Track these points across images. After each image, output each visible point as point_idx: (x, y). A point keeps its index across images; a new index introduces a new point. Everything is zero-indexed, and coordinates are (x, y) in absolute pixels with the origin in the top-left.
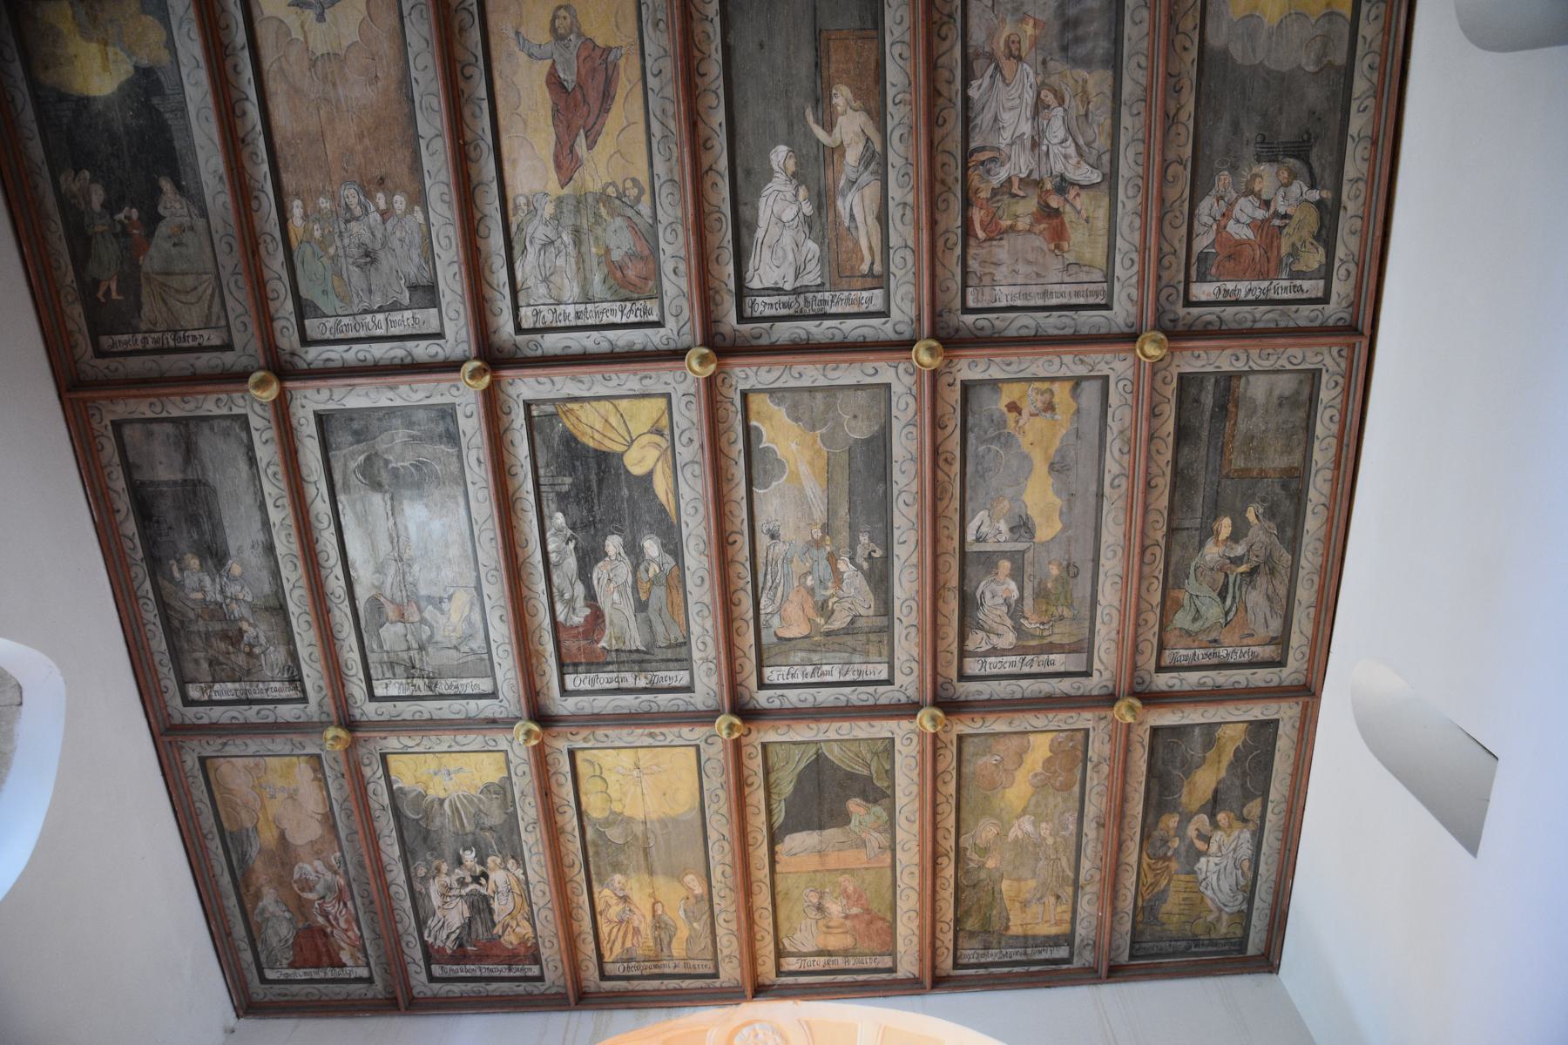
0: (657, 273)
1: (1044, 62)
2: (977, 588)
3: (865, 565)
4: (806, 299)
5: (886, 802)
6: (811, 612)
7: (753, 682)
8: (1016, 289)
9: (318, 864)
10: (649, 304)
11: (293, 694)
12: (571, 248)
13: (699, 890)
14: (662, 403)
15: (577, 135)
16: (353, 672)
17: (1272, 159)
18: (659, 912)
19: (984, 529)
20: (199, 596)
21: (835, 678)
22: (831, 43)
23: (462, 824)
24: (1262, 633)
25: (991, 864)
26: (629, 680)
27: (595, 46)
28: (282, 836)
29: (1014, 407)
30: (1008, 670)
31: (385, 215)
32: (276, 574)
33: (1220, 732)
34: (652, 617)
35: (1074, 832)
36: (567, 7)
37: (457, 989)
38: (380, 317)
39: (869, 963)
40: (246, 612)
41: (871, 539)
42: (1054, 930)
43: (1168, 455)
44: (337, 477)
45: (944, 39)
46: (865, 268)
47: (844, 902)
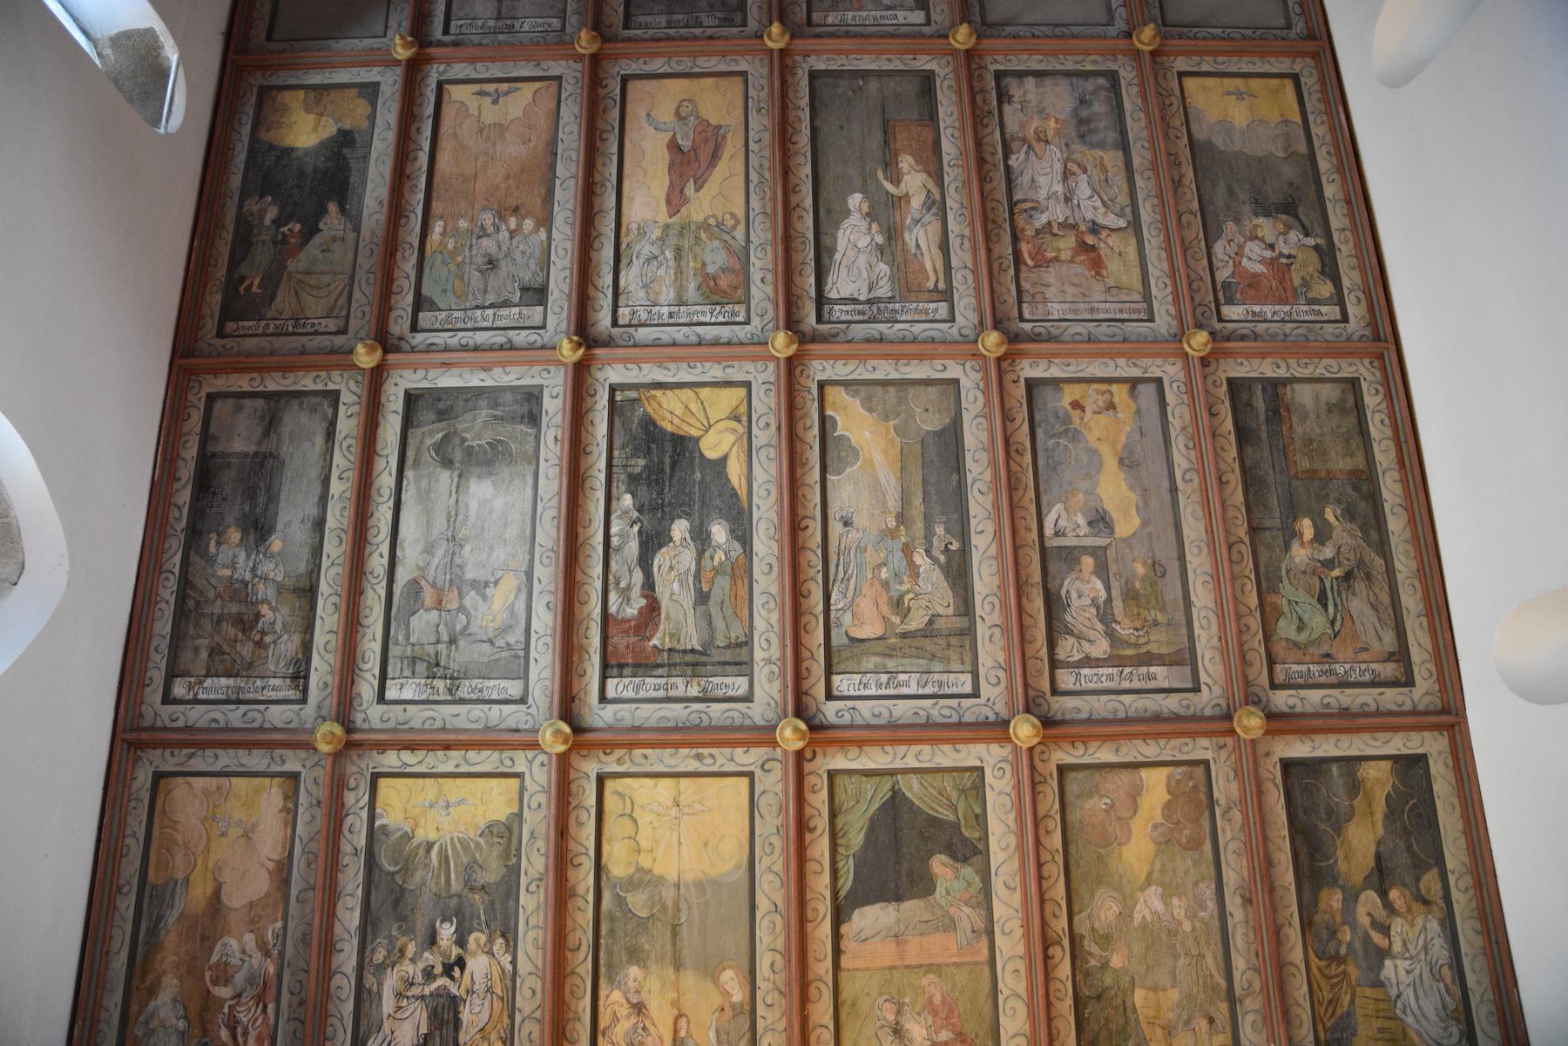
2: (1061, 586)
3: (942, 558)
4: (878, 308)
6: (886, 609)
10: (737, 308)
12: (671, 263)
13: (738, 995)
14: (742, 392)
18: (683, 1033)
19: (1062, 523)
21: (912, 690)
24: (1376, 646)
25: (1116, 961)
27: (709, 124)
29: (1076, 405)
32: (317, 551)
35: (1216, 913)
36: (689, 101)
38: (490, 312)
40: (271, 593)
41: (947, 531)
46: (931, 285)
47: (930, 1019)
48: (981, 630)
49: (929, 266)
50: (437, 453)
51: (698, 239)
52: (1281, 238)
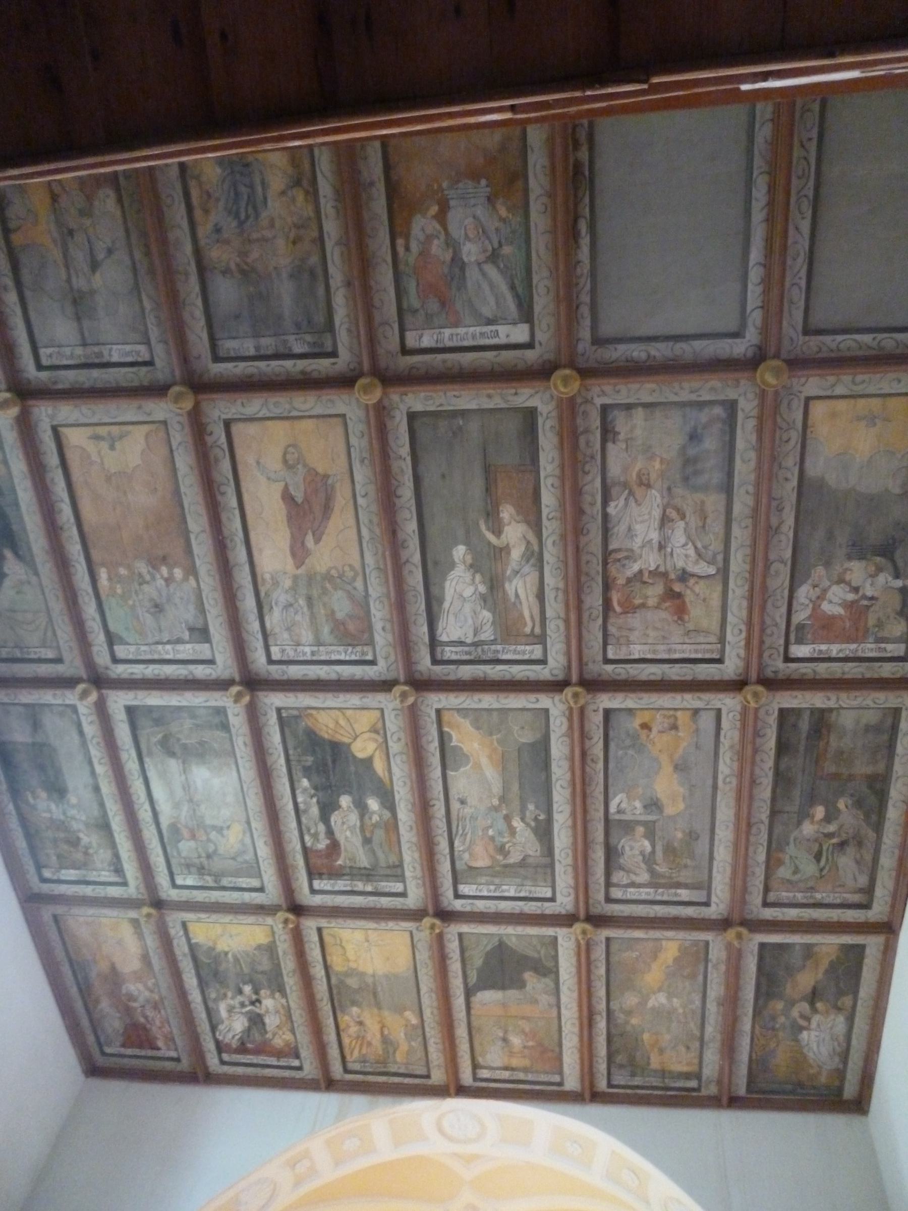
0: (370, 628)
1: (669, 489)
2: (619, 842)
3: (533, 824)
4: (483, 650)
5: (553, 976)
6: (491, 851)
7: (450, 894)
8: (646, 647)
9: (140, 986)
10: (365, 649)
11: (114, 878)
12: (305, 609)
13: (414, 1021)
14: (377, 714)
15: (306, 534)
16: (160, 869)
17: (861, 557)
19: (623, 805)
20: (47, 815)
21: (512, 893)
22: (498, 475)
23: (241, 968)
24: (850, 883)
26: (360, 886)
27: (317, 473)
28: (113, 968)
29: (645, 726)
30: (644, 897)
31: (168, 581)
32: (102, 805)
33: (816, 949)
34: (376, 849)
36: (294, 446)
37: (240, 1070)
38: (168, 647)
39: (543, 1078)
40: (82, 827)
41: (537, 807)
42: (685, 1069)
43: (770, 763)
44: (143, 746)
45: (588, 473)
46: (528, 630)
48: (558, 868)
49: (527, 614)
50: (162, 746)
51: (325, 592)
52: (869, 581)
